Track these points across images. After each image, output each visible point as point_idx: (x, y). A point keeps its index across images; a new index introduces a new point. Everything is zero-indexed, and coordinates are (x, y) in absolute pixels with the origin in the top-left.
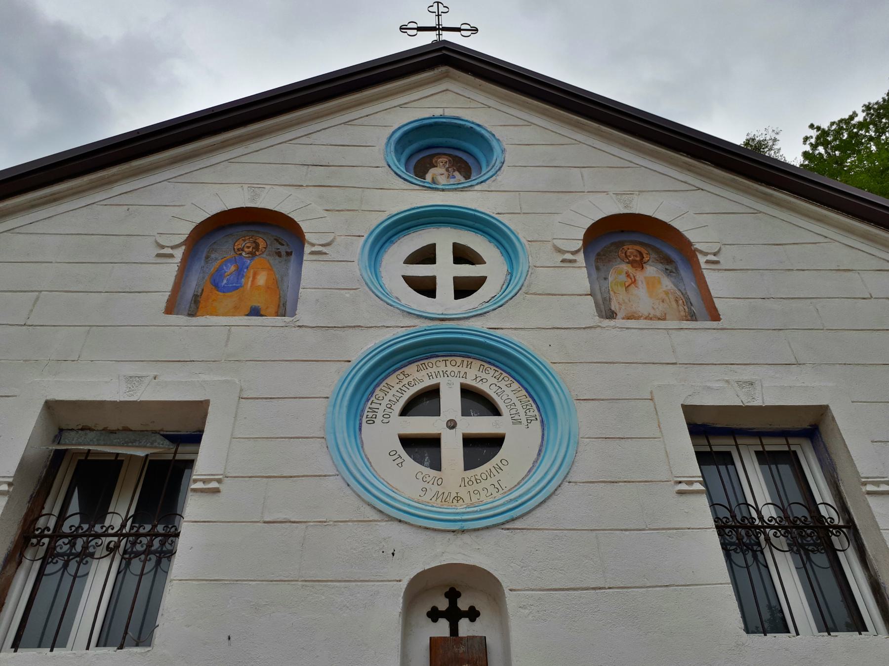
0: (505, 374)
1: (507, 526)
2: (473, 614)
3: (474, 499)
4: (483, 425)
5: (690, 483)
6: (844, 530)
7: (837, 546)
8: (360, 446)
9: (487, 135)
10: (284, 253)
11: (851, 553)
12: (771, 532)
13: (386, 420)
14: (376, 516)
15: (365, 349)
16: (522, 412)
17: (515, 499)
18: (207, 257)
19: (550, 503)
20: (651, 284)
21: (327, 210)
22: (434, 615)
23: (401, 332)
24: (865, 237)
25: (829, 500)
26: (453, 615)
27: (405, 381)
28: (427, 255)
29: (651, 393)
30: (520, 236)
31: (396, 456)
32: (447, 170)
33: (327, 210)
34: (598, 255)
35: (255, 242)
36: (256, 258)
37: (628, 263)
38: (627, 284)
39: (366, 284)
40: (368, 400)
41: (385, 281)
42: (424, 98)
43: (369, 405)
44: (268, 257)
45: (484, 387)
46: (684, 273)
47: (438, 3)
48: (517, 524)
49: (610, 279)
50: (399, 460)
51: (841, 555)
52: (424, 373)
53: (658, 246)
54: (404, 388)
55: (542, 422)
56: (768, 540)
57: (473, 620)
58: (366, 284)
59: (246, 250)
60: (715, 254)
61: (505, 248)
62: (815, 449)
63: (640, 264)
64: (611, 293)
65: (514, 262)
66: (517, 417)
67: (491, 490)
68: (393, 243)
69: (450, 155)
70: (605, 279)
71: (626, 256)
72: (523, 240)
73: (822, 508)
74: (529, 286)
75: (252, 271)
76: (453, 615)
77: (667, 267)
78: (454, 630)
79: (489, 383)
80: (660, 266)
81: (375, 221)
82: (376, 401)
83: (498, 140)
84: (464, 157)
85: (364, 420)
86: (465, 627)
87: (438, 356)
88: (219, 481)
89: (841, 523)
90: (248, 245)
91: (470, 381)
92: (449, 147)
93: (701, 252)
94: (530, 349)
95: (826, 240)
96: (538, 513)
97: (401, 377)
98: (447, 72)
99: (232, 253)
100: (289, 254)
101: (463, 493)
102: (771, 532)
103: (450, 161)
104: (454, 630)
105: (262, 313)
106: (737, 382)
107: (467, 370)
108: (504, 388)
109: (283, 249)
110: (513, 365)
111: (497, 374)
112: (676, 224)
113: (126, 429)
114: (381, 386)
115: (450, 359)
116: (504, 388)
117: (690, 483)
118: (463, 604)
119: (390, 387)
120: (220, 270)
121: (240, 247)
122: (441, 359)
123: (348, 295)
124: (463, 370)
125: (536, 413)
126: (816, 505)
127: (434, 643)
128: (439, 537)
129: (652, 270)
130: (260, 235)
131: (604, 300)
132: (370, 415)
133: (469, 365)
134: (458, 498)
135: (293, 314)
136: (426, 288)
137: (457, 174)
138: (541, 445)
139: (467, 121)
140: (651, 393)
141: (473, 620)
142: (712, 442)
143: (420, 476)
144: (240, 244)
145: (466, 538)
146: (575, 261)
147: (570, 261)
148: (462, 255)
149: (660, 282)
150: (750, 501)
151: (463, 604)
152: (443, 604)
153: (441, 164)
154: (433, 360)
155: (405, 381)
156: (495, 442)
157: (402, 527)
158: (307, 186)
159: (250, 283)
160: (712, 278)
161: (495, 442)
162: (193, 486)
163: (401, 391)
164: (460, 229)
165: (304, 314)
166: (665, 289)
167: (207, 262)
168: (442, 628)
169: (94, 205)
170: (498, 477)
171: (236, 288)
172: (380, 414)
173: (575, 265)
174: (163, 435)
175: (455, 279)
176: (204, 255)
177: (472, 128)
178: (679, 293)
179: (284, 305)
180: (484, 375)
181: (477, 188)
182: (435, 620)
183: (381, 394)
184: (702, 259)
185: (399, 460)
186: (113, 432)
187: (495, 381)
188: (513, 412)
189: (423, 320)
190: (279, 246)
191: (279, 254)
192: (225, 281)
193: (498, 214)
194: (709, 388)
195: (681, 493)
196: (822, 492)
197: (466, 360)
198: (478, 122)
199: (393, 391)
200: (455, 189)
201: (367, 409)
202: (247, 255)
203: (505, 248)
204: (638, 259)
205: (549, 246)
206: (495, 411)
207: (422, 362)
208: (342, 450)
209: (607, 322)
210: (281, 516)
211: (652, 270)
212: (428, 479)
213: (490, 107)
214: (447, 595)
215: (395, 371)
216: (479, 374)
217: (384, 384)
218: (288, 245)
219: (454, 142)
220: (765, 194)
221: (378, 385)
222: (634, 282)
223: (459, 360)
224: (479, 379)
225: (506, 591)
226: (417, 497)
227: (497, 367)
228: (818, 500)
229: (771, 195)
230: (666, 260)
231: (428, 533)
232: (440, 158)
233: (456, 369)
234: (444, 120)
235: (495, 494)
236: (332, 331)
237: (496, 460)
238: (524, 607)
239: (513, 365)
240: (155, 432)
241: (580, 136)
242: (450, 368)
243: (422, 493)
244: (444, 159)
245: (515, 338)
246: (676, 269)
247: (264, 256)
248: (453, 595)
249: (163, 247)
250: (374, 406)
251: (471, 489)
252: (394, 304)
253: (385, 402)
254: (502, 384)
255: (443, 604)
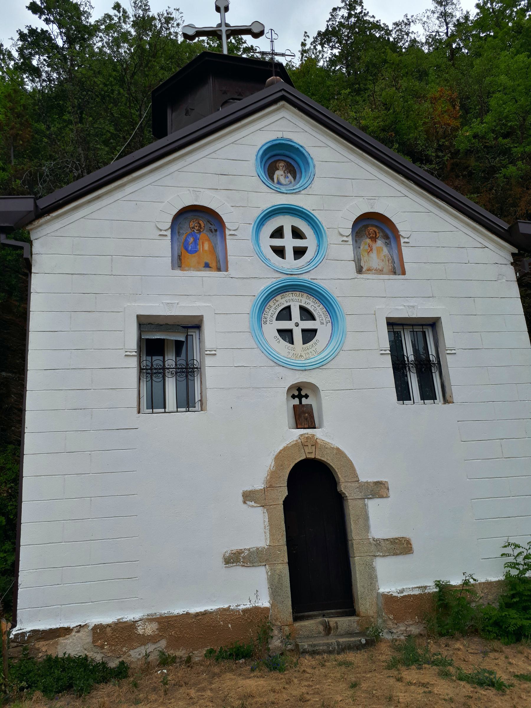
0: (317, 301)
1: (320, 368)
2: (306, 396)
3: (307, 356)
4: (309, 325)
5: (385, 350)
6: (437, 365)
7: (433, 371)
8: (263, 334)
9: (306, 154)
10: (213, 230)
11: (437, 373)
12: (410, 365)
13: (271, 323)
14: (274, 365)
15: (260, 290)
16: (324, 318)
17: (323, 358)
18: (179, 233)
19: (335, 358)
20: (379, 250)
21: (232, 206)
22: (294, 397)
23: (274, 280)
24: (474, 229)
25: (434, 353)
26: (300, 397)
27: (277, 304)
28: (278, 233)
29: (375, 311)
30: (324, 225)
31: (277, 339)
32: (284, 172)
33: (232, 206)
34: (357, 233)
35: (199, 223)
36: (202, 234)
37: (369, 238)
38: (368, 251)
39: (257, 254)
40: (263, 313)
41: (263, 249)
42: (272, 123)
43: (263, 316)
44: (207, 233)
45: (308, 307)
46: (393, 244)
47: (271, 30)
48: (324, 367)
49: (361, 248)
50: (278, 340)
51: (433, 374)
52: (284, 300)
53: (382, 227)
54: (276, 307)
55: (332, 323)
56: (409, 369)
57: (307, 398)
58: (257, 254)
59: (196, 228)
60: (408, 238)
61: (316, 231)
62: (433, 331)
63: (374, 239)
64: (362, 256)
65: (320, 240)
66: (322, 321)
67: (313, 352)
68: (264, 225)
69: (285, 161)
70: (359, 248)
71: (369, 234)
72: (325, 228)
73: (431, 356)
74: (328, 255)
75: (201, 241)
76: (300, 397)
77: (387, 241)
78: (300, 402)
79: (311, 305)
80: (384, 241)
81: (256, 213)
82: (266, 313)
83: (312, 158)
84: (293, 163)
85: (263, 322)
86: (304, 401)
87: (289, 291)
88: (215, 351)
89: (436, 362)
90: (196, 225)
91: (303, 304)
92: (284, 156)
93: (402, 236)
94: (330, 292)
95: (457, 230)
96: (331, 363)
97: (275, 302)
98: (284, 105)
99: (190, 230)
100: (216, 231)
101: (303, 354)
102: (410, 365)
103: (285, 165)
104: (300, 402)
105: (210, 266)
106: (408, 306)
107: (302, 298)
108: (317, 307)
109: (213, 227)
110: (321, 297)
111: (314, 300)
112: (393, 220)
113: (167, 324)
114: (267, 307)
115: (294, 292)
116: (317, 307)
117: (385, 350)
118: (303, 393)
119: (271, 307)
120: (186, 240)
121: (192, 226)
122: (290, 293)
123: (249, 260)
124: (300, 298)
125: (330, 319)
126: (429, 355)
127: (295, 407)
128: (297, 372)
129: (380, 243)
130: (200, 219)
131: (358, 260)
132: (265, 320)
133: (302, 296)
134: (301, 356)
135: (227, 270)
136: (280, 252)
137: (289, 175)
138: (332, 334)
139: (295, 143)
140: (375, 311)
141: (307, 398)
142: (394, 328)
143: (287, 347)
144: (192, 224)
145: (306, 372)
146: (348, 241)
147: (346, 241)
148: (297, 234)
149: (382, 250)
150: (405, 354)
151: (303, 393)
152: (296, 393)
153: (281, 168)
154: (287, 293)
155: (277, 304)
156: (314, 332)
157: (284, 368)
158: (220, 189)
159: (201, 249)
160: (405, 251)
161: (314, 332)
162: (206, 353)
163: (276, 309)
164: (295, 217)
165: (232, 271)
166: (384, 254)
167: (179, 235)
168: (296, 401)
169: (119, 201)
170: (316, 347)
171: (196, 251)
172: (268, 320)
173: (348, 243)
174: (182, 326)
175: (293, 247)
176: (177, 231)
177: (298, 148)
178: (390, 256)
179: (219, 261)
180: (308, 301)
181: (303, 192)
182: (294, 399)
183: (268, 310)
184: (402, 240)
185: (278, 340)
186: (161, 325)
187: (313, 304)
188: (321, 319)
189: (283, 275)
190: (211, 226)
191: (211, 231)
192: (190, 248)
193: (313, 210)
194: (397, 309)
195: (382, 354)
196: (432, 350)
197: (301, 293)
198: (301, 144)
199: (272, 309)
200: (292, 193)
201: (263, 318)
202: (197, 232)
203: (316, 231)
204: (374, 236)
205: (337, 232)
206: (313, 319)
207: (283, 294)
208: (258, 338)
209: (360, 276)
210: (240, 365)
211: (380, 243)
212: (290, 348)
213: (306, 132)
214: (297, 390)
215: (272, 299)
216: (307, 300)
217: (268, 305)
218: (214, 225)
219: (287, 153)
220: (435, 202)
221: (266, 306)
222: (371, 250)
223: (298, 293)
224: (306, 303)
225: (321, 391)
226: (286, 356)
227: (314, 297)
228: (430, 353)
229: (438, 203)
230: (386, 237)
231: (293, 370)
232: (280, 163)
233: (297, 298)
234: (283, 142)
235: (315, 354)
236: (245, 280)
237: (314, 340)
238: (327, 396)
239: (321, 297)
240: (178, 325)
241: (352, 157)
242: (294, 298)
243: (288, 354)
244: (282, 164)
245: (322, 284)
246: (390, 242)
247: (205, 232)
248: (299, 390)
249: (161, 230)
250: (265, 316)
251: (306, 352)
252: (270, 266)
253: (270, 314)
254: (316, 305)
255: (296, 393)
